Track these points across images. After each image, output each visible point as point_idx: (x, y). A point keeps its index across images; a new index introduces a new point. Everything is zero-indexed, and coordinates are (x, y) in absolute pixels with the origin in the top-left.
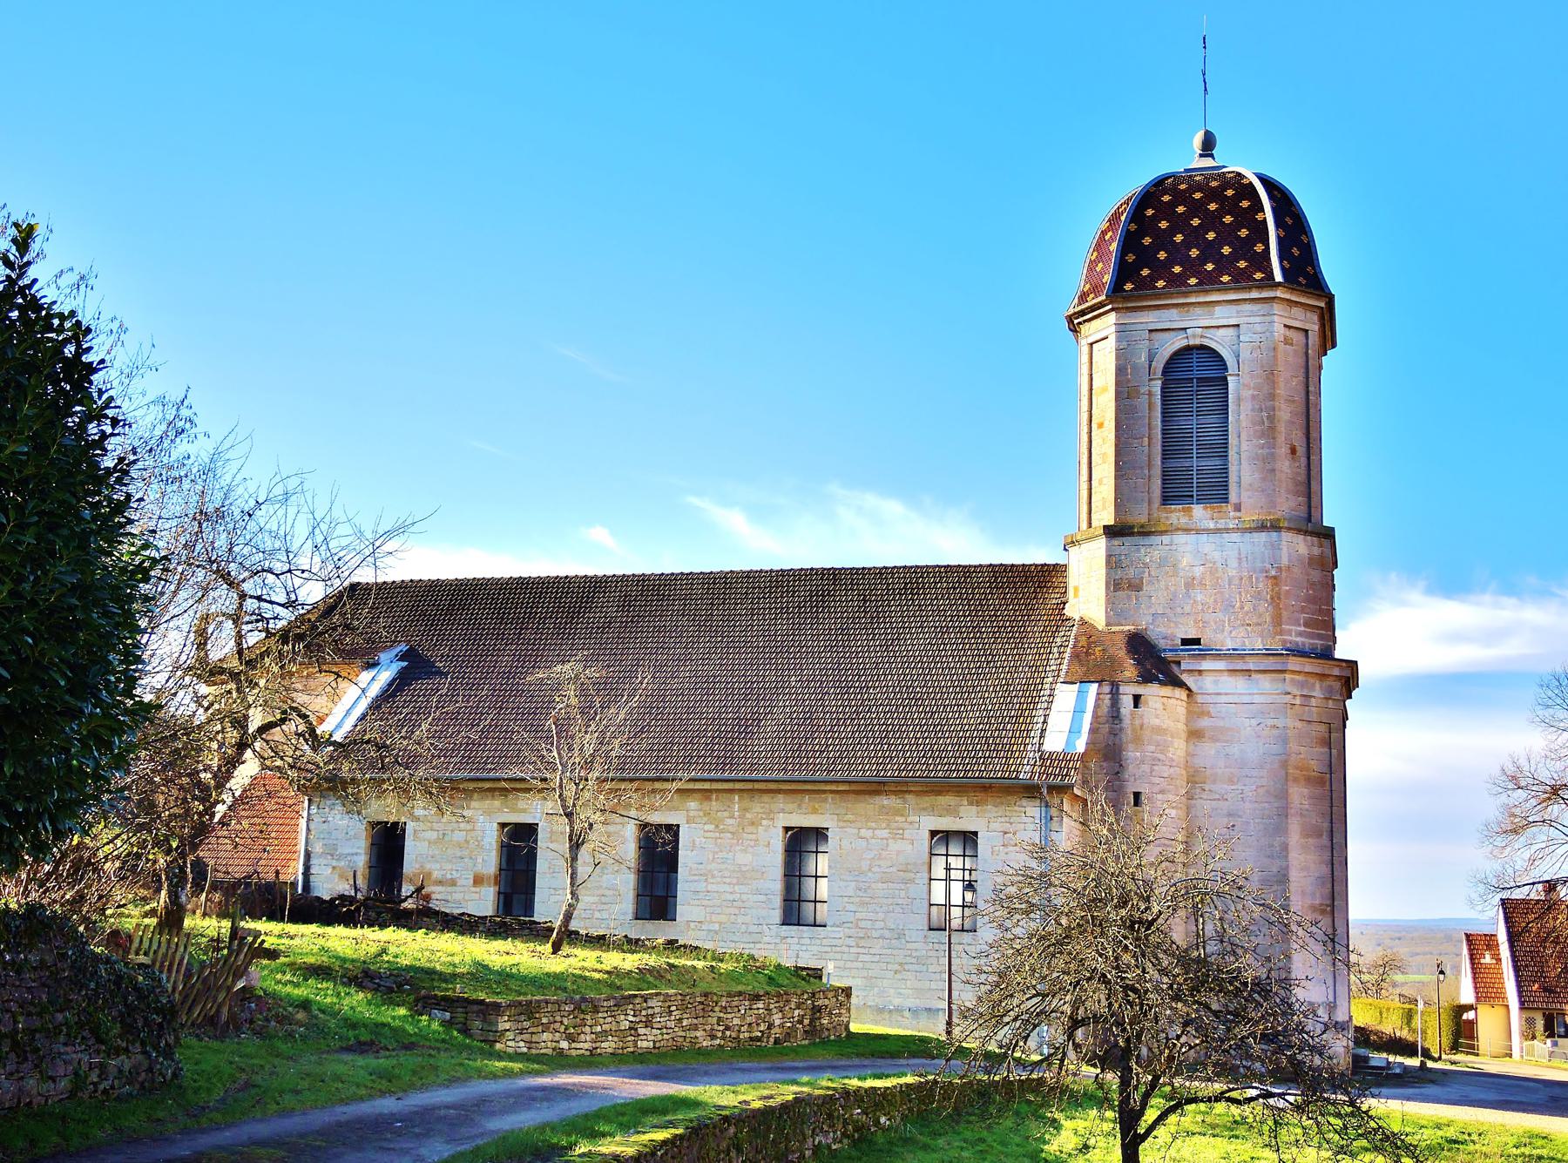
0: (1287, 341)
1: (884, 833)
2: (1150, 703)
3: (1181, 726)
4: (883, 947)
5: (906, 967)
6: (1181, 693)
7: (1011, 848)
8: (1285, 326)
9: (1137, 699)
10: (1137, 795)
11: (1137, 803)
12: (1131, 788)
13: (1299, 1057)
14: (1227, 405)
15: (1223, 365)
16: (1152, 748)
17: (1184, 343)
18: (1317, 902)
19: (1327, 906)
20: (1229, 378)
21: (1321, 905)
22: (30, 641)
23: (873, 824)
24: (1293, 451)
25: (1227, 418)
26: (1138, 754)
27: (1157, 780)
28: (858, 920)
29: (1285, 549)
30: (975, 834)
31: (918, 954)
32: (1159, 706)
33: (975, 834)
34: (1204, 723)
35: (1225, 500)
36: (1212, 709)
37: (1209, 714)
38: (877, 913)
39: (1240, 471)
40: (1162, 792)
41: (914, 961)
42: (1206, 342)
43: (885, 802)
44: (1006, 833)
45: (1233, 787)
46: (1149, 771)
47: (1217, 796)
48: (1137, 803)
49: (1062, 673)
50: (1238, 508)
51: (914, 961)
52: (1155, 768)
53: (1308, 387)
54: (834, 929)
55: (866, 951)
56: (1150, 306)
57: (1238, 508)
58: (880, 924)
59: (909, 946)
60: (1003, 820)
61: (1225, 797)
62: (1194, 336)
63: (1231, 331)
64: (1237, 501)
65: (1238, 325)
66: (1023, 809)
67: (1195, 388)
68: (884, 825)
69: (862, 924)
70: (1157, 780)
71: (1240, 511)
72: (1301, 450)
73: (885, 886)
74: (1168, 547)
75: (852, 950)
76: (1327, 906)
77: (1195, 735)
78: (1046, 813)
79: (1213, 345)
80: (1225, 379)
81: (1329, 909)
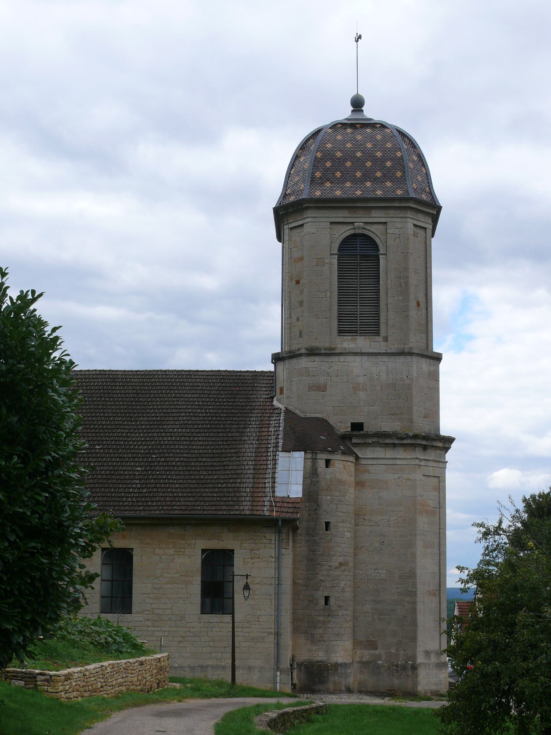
0: (415, 235)
1: (171, 551)
2: (336, 465)
3: (353, 479)
4: (170, 627)
5: (186, 639)
6: (352, 459)
7: (256, 560)
8: (415, 225)
9: (328, 463)
10: (327, 524)
11: (327, 528)
12: (324, 519)
13: (86, 524)
14: (379, 273)
15: (376, 247)
16: (337, 494)
17: (352, 232)
18: (431, 589)
19: (437, 591)
20: (380, 256)
21: (433, 590)
22: (42, 637)
23: (164, 546)
24: (418, 304)
25: (379, 281)
26: (329, 497)
27: (340, 514)
28: (153, 609)
29: (415, 366)
30: (232, 551)
31: (194, 630)
32: (341, 466)
33: (232, 551)
34: (365, 477)
35: (378, 333)
36: (371, 468)
37: (368, 471)
38: (167, 604)
39: (387, 316)
40: (343, 522)
41: (191, 634)
42: (366, 232)
43: (172, 531)
44: (252, 550)
45: (383, 518)
46: (335, 508)
47: (373, 524)
48: (327, 528)
49: (280, 444)
50: (386, 339)
51: (191, 634)
52: (338, 506)
53: (426, 264)
54: (137, 615)
55: (159, 629)
56: (333, 207)
57: (386, 339)
58: (169, 612)
59: (189, 625)
60: (250, 541)
61: (378, 524)
62: (359, 228)
63: (381, 227)
64: (385, 335)
65: (385, 223)
66: (264, 535)
67: (359, 261)
68: (171, 546)
69: (156, 611)
70: (340, 514)
71: (387, 341)
72: (422, 305)
73: (172, 586)
74: (343, 363)
75: (149, 629)
76: (437, 591)
77: (359, 484)
78: (279, 537)
79: (370, 234)
80: (378, 257)
81: (437, 592)
